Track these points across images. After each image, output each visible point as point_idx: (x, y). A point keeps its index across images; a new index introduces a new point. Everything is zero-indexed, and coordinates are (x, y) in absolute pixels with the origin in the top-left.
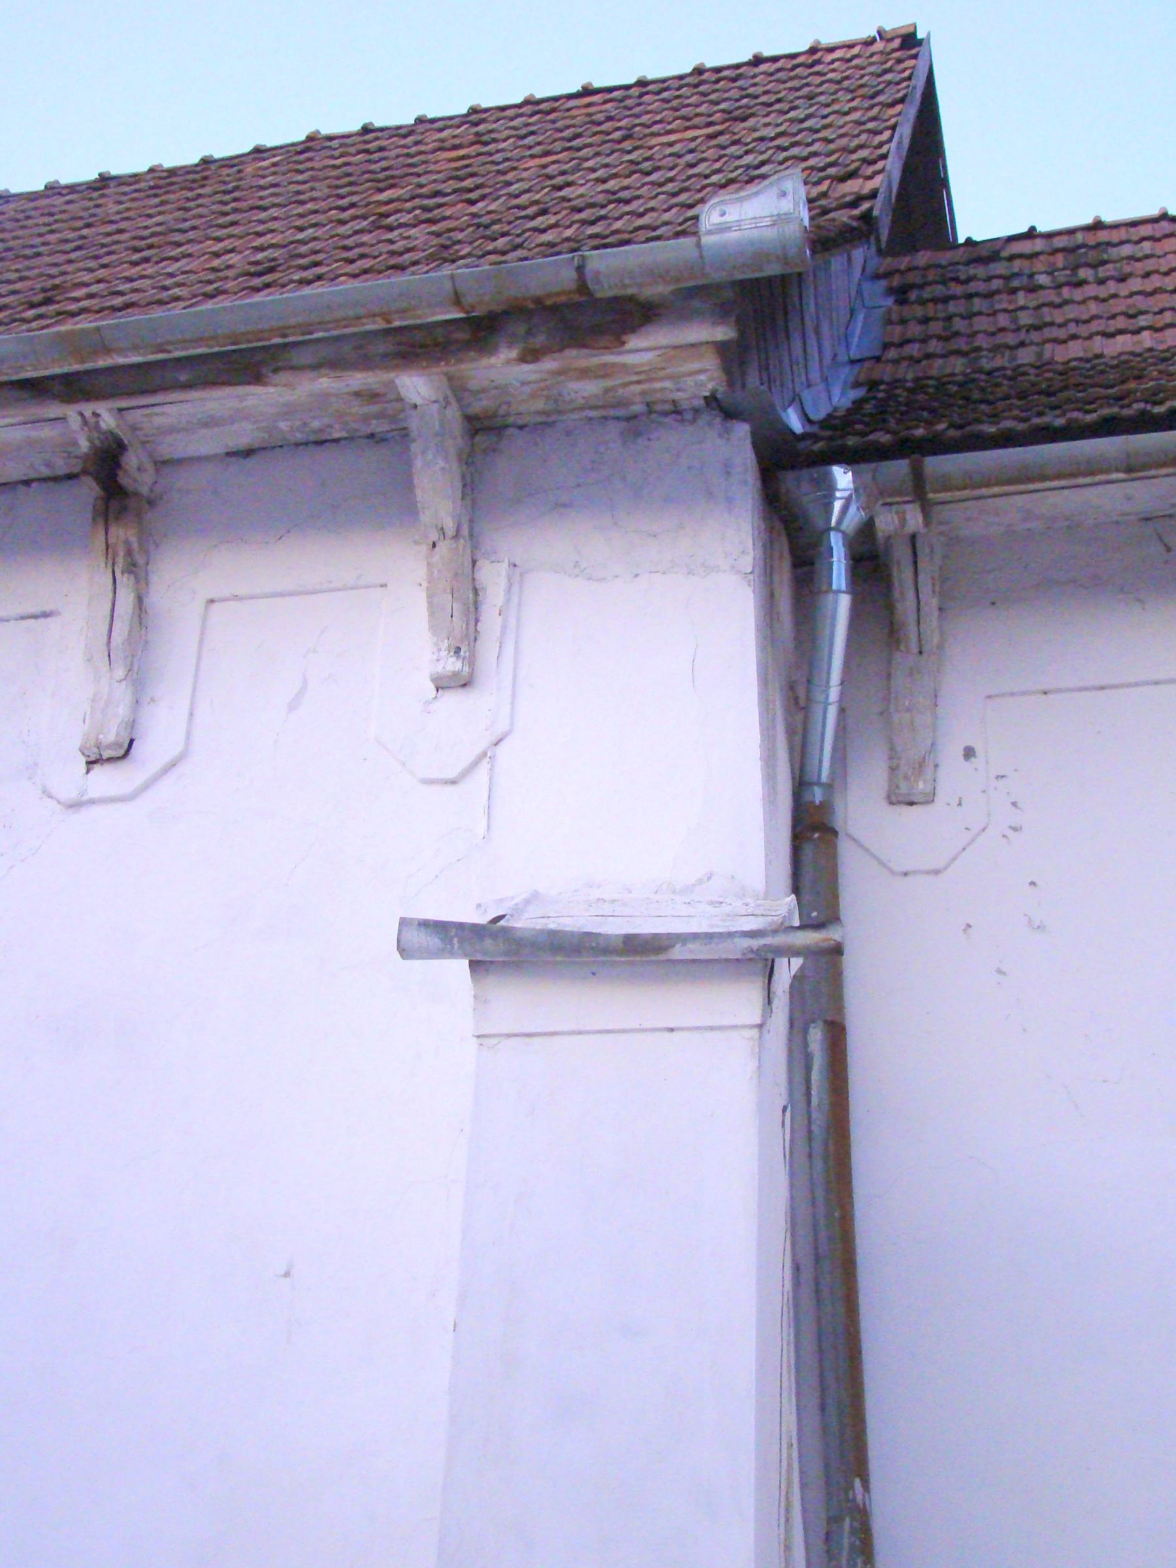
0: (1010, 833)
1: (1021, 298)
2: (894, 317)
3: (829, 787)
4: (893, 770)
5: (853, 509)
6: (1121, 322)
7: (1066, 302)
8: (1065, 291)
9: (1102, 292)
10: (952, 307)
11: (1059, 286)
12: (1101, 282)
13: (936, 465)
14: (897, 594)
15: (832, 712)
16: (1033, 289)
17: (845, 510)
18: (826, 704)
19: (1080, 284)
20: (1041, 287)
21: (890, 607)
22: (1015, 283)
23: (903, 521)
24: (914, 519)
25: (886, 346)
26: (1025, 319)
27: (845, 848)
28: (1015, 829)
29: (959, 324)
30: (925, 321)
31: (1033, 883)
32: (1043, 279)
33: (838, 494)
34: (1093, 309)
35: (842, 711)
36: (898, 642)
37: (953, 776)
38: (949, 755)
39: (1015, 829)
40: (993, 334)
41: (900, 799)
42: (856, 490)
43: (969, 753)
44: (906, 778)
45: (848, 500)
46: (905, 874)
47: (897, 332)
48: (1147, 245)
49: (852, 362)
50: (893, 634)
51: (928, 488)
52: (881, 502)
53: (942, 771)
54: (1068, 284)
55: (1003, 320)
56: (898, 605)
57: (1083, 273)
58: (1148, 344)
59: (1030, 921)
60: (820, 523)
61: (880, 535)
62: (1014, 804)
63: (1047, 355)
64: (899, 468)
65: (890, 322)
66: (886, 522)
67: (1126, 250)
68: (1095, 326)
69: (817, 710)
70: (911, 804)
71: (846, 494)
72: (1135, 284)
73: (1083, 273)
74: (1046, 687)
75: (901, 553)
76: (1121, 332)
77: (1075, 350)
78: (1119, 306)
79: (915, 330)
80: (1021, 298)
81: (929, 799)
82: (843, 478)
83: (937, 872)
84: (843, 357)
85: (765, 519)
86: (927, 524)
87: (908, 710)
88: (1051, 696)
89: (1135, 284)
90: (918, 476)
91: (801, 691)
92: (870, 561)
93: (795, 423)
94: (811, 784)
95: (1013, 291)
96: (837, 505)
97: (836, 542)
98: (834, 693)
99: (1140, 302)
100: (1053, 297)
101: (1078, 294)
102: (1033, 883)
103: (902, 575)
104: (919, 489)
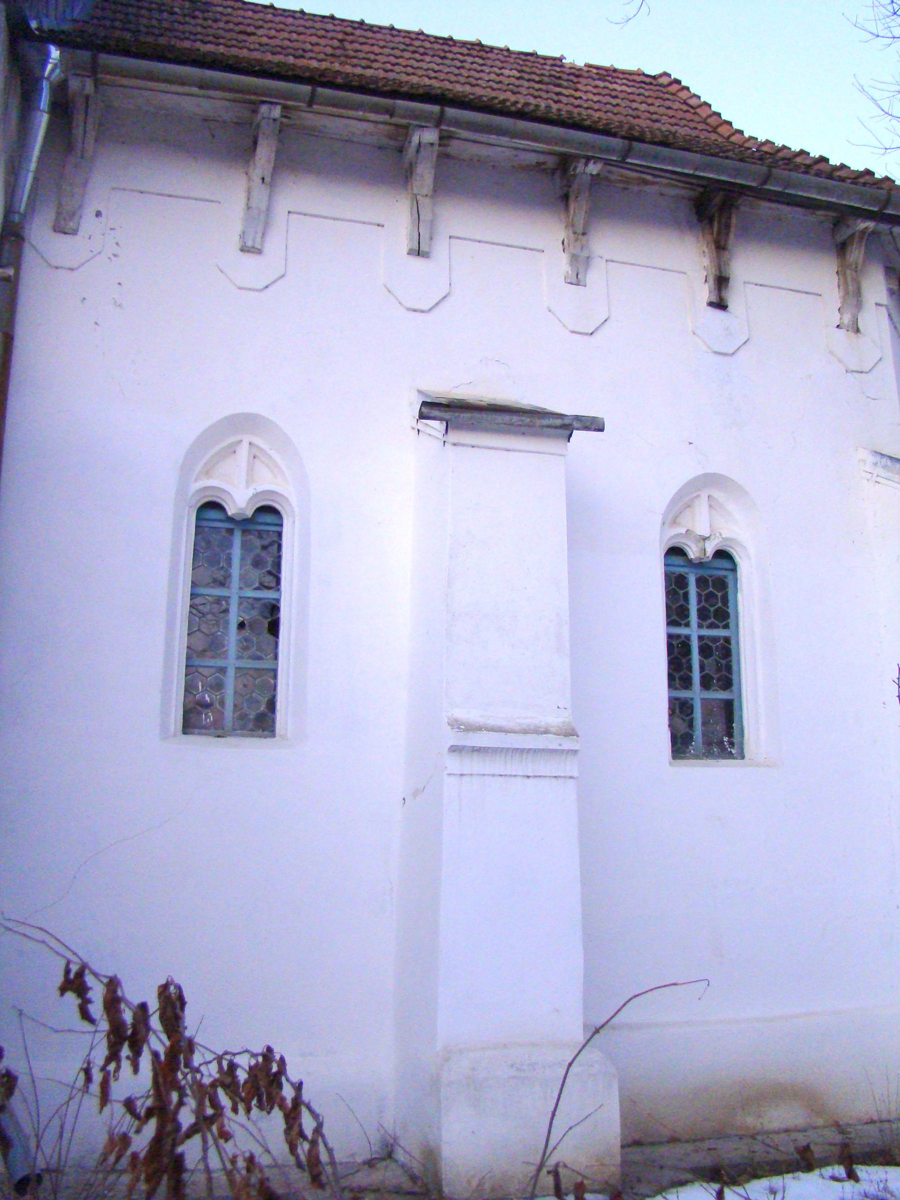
0: (113, 258)
1: (165, 15)
2: (100, 6)
3: (24, 216)
4: (58, 214)
5: (58, 71)
6: (211, 38)
7: (186, 23)
8: (187, 19)
9: (205, 24)
10: (130, 10)
11: (185, 16)
12: (205, 19)
13: (105, 59)
14: (74, 124)
15: (30, 177)
16: (172, 13)
17: (53, 70)
18: (28, 171)
19: (194, 17)
20: (176, 13)
21: (70, 130)
22: (163, 8)
23: (83, 87)
24: (89, 87)
25: (92, 18)
26: (165, 25)
27: (27, 248)
28: (115, 255)
29: (131, 18)
30: (115, 12)
31: (119, 284)
32: (176, 10)
33: (51, 61)
34: (199, 29)
35: (36, 179)
36: (72, 149)
37: (88, 224)
38: (89, 212)
39: (115, 255)
40: (148, 27)
41: (59, 229)
42: (60, 61)
43: (98, 214)
44: (64, 219)
45: (56, 66)
46: (57, 268)
47: (99, 13)
48: (229, 10)
49: (74, 20)
50: (70, 147)
51: (99, 70)
52: (73, 72)
53: (83, 221)
54: (189, 16)
55: (154, 22)
56: (74, 131)
57: (197, 13)
58: (222, 51)
59: (116, 302)
60: (37, 73)
61: (70, 92)
62: (117, 244)
63: (173, 43)
64: (86, 55)
65: (97, 7)
66: (74, 84)
67: (220, 9)
68: (199, 37)
69: (23, 172)
70: (65, 233)
71: (55, 62)
72: (221, 25)
73: (197, 13)
74: (142, 190)
75: (80, 104)
76: (210, 42)
77: (187, 44)
78: (211, 31)
79: (109, 14)
80: (165, 15)
81: (75, 232)
82: (55, 53)
83: (72, 269)
84: (69, 18)
85: (8, 63)
86: (96, 91)
87: (71, 184)
88: (144, 195)
89: (221, 25)
90: (94, 59)
91: (16, 163)
92: (62, 108)
93: (34, 25)
94: (15, 213)
95: (162, 12)
96: (49, 67)
97: (45, 85)
98: (33, 166)
99: (222, 33)
100: (180, 19)
101: (192, 21)
102: (119, 284)
103: (79, 118)
104: (94, 70)
